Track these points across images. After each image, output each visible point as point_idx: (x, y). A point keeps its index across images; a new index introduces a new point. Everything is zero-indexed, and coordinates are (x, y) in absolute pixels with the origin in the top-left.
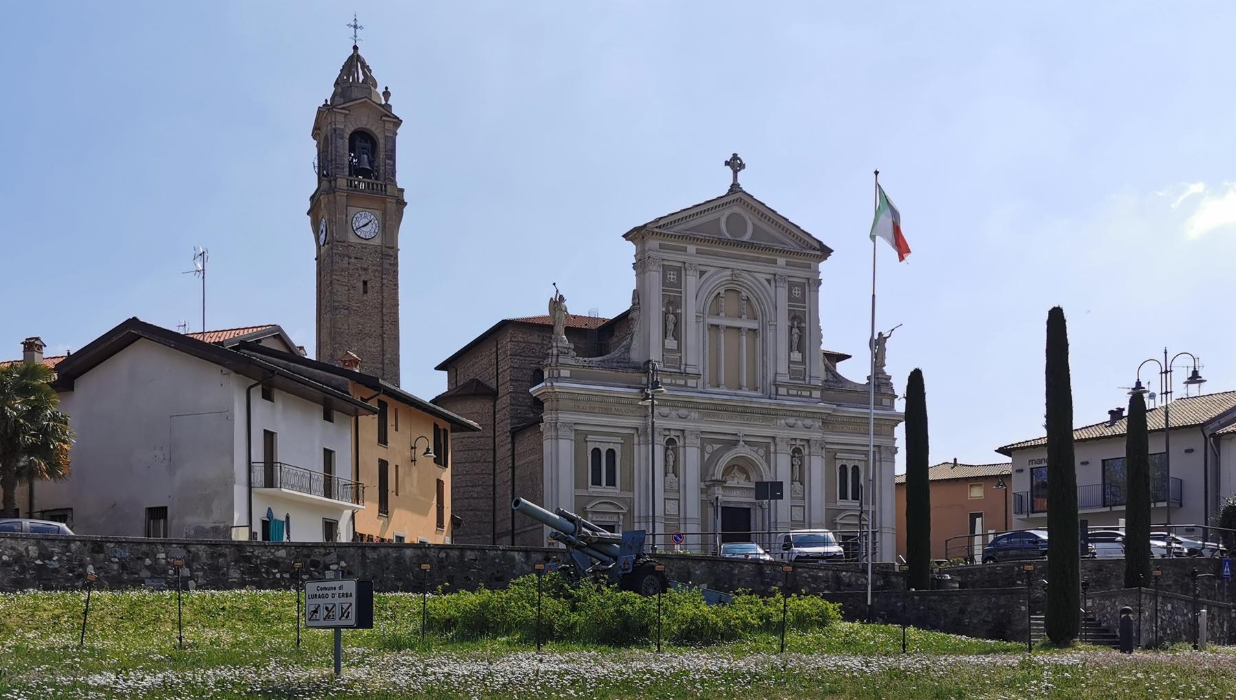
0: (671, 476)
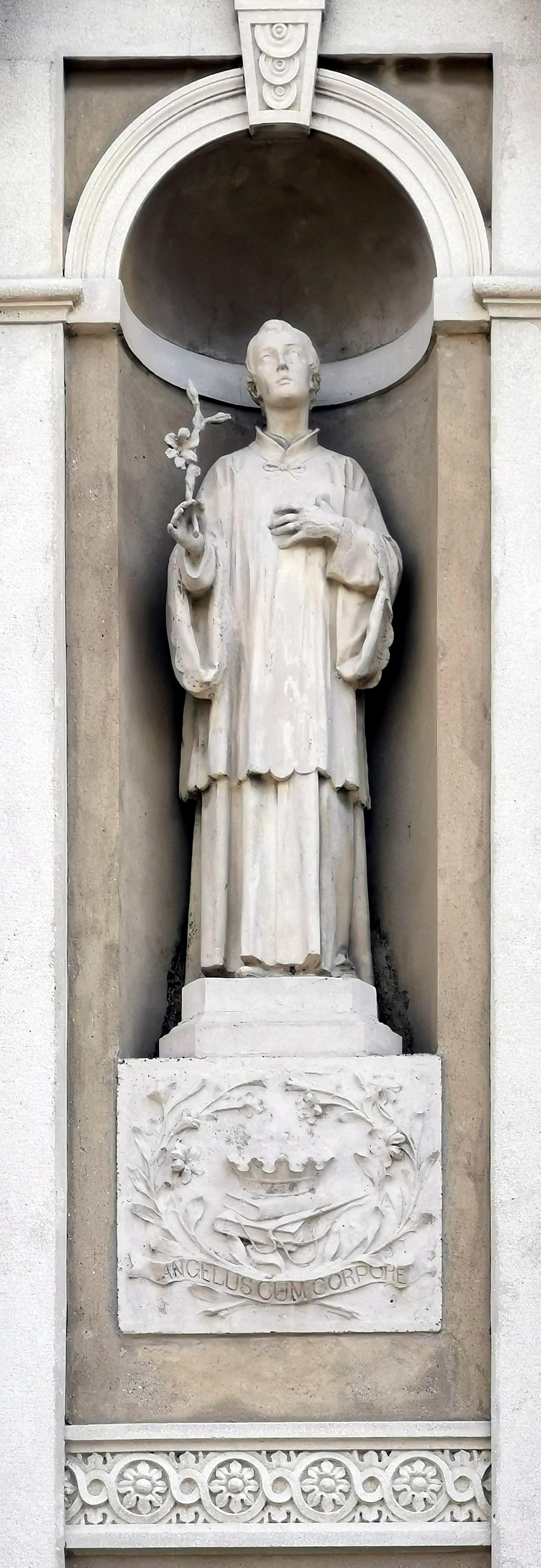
0: (282, 1033)
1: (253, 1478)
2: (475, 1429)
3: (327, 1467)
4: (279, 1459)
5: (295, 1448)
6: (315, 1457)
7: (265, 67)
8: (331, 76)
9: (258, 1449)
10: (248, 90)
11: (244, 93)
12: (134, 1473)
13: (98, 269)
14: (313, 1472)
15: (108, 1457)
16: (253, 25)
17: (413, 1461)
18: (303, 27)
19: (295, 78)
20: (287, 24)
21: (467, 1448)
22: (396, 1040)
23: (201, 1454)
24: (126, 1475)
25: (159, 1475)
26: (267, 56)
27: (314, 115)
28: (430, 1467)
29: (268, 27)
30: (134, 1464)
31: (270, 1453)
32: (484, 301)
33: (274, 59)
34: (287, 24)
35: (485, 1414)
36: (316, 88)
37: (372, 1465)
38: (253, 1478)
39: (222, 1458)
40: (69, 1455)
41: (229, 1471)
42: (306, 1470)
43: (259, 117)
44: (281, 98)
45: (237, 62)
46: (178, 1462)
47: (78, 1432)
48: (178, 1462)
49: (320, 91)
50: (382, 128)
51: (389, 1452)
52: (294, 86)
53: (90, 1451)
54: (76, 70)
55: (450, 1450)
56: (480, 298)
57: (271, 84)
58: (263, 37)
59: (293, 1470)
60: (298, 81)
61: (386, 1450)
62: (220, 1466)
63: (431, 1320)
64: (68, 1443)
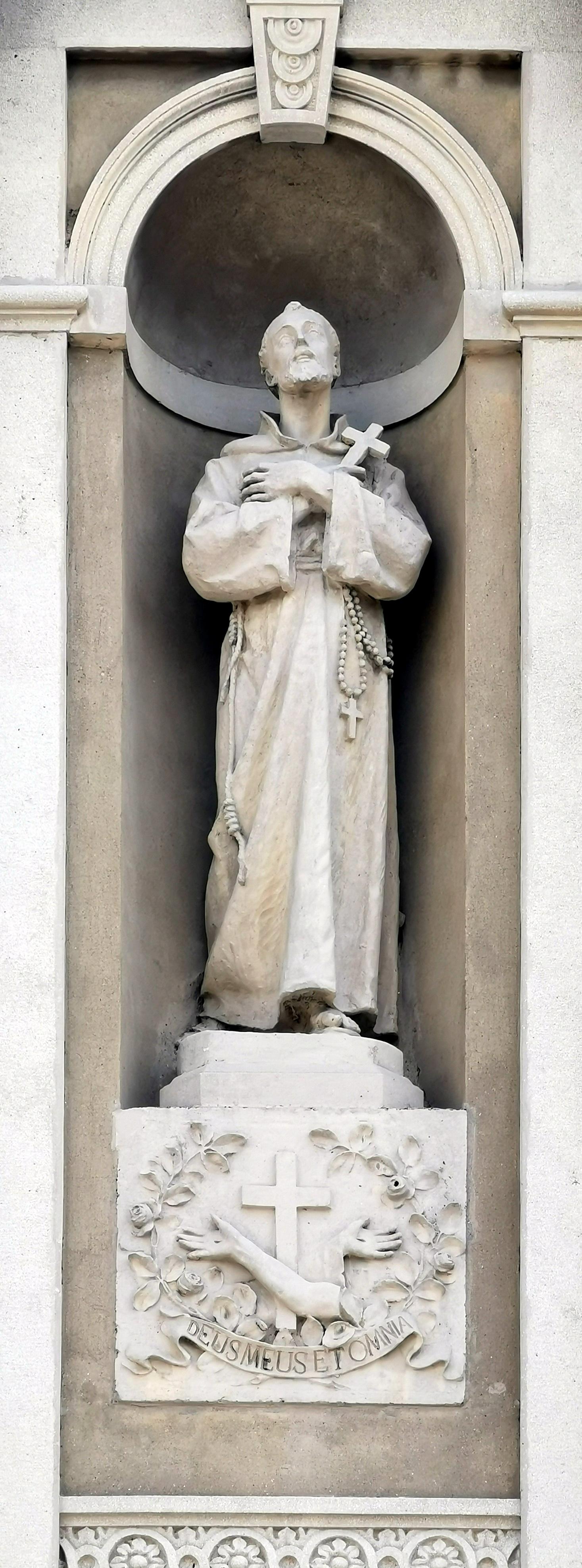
1: (159, 1556)
2: (505, 1507)
3: (339, 1545)
4: (187, 1535)
5: (404, 1524)
6: (423, 1536)
7: (280, 66)
8: (350, 75)
9: (165, 1524)
10: (259, 91)
11: (255, 94)
12: (229, 1549)
13: (94, 272)
14: (424, 1552)
15: (100, 1531)
16: (266, 21)
17: (434, 1539)
18: (321, 22)
19: (310, 76)
20: (301, 20)
21: (292, 1525)
22: (417, 1093)
23: (301, 1530)
24: (221, 1551)
25: (356, 1553)
26: (280, 53)
27: (332, 117)
28: (451, 1548)
29: (282, 22)
30: (128, 1540)
31: (176, 1529)
32: (515, 318)
33: (288, 56)
34: (301, 20)
35: (515, 1493)
36: (333, 87)
37: (388, 1545)
38: (159, 1556)
39: (224, 1534)
40: (63, 1529)
41: (333, 1548)
42: (116, 1546)
43: (270, 116)
44: (292, 98)
45: (243, 58)
46: (177, 1537)
47: (76, 1504)
48: (177, 1537)
49: (338, 91)
50: (408, 133)
51: (105, 1528)
52: (310, 86)
53: (180, 1525)
54: (82, 63)
55: (173, 1527)
56: (510, 315)
57: (284, 82)
58: (276, 31)
59: (101, 1547)
60: (313, 79)
61: (403, 1529)
62: (223, 1542)
63: (458, 1394)
64: (63, 1516)
